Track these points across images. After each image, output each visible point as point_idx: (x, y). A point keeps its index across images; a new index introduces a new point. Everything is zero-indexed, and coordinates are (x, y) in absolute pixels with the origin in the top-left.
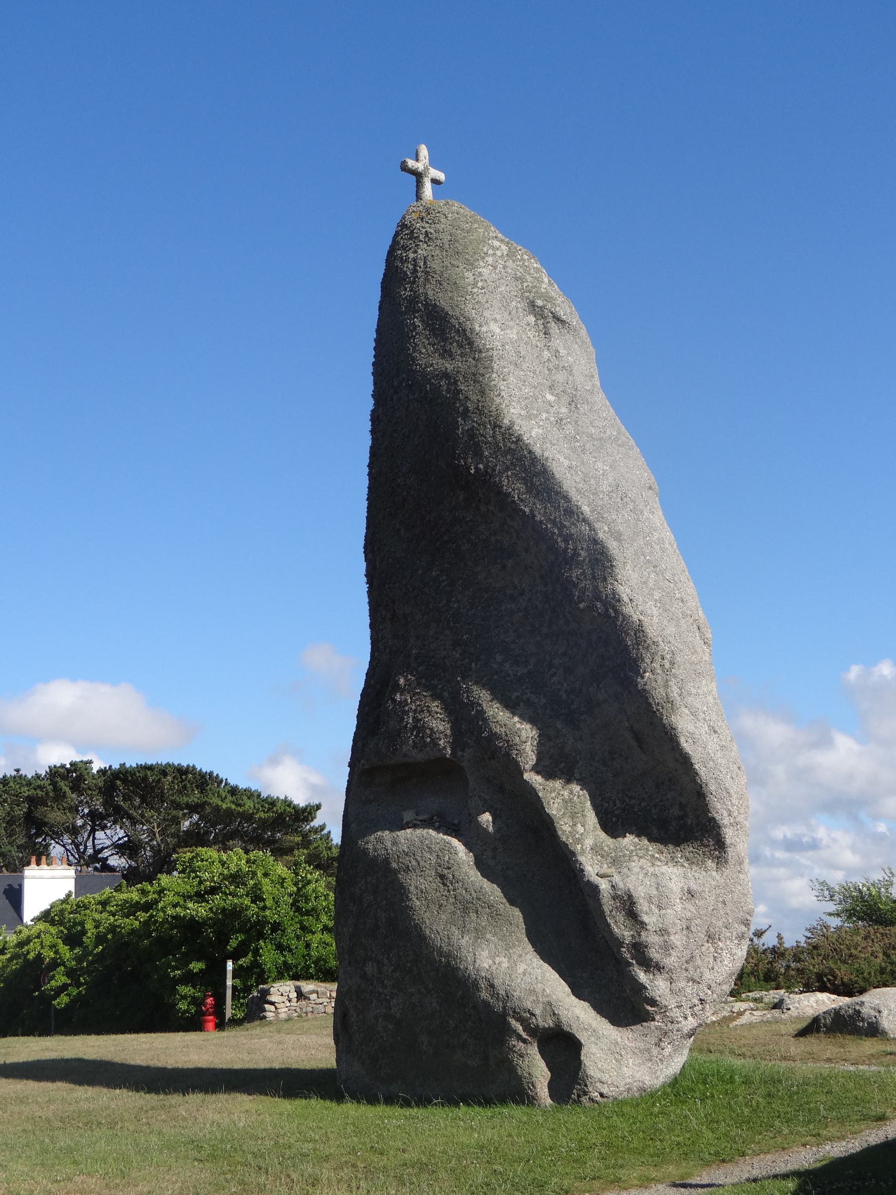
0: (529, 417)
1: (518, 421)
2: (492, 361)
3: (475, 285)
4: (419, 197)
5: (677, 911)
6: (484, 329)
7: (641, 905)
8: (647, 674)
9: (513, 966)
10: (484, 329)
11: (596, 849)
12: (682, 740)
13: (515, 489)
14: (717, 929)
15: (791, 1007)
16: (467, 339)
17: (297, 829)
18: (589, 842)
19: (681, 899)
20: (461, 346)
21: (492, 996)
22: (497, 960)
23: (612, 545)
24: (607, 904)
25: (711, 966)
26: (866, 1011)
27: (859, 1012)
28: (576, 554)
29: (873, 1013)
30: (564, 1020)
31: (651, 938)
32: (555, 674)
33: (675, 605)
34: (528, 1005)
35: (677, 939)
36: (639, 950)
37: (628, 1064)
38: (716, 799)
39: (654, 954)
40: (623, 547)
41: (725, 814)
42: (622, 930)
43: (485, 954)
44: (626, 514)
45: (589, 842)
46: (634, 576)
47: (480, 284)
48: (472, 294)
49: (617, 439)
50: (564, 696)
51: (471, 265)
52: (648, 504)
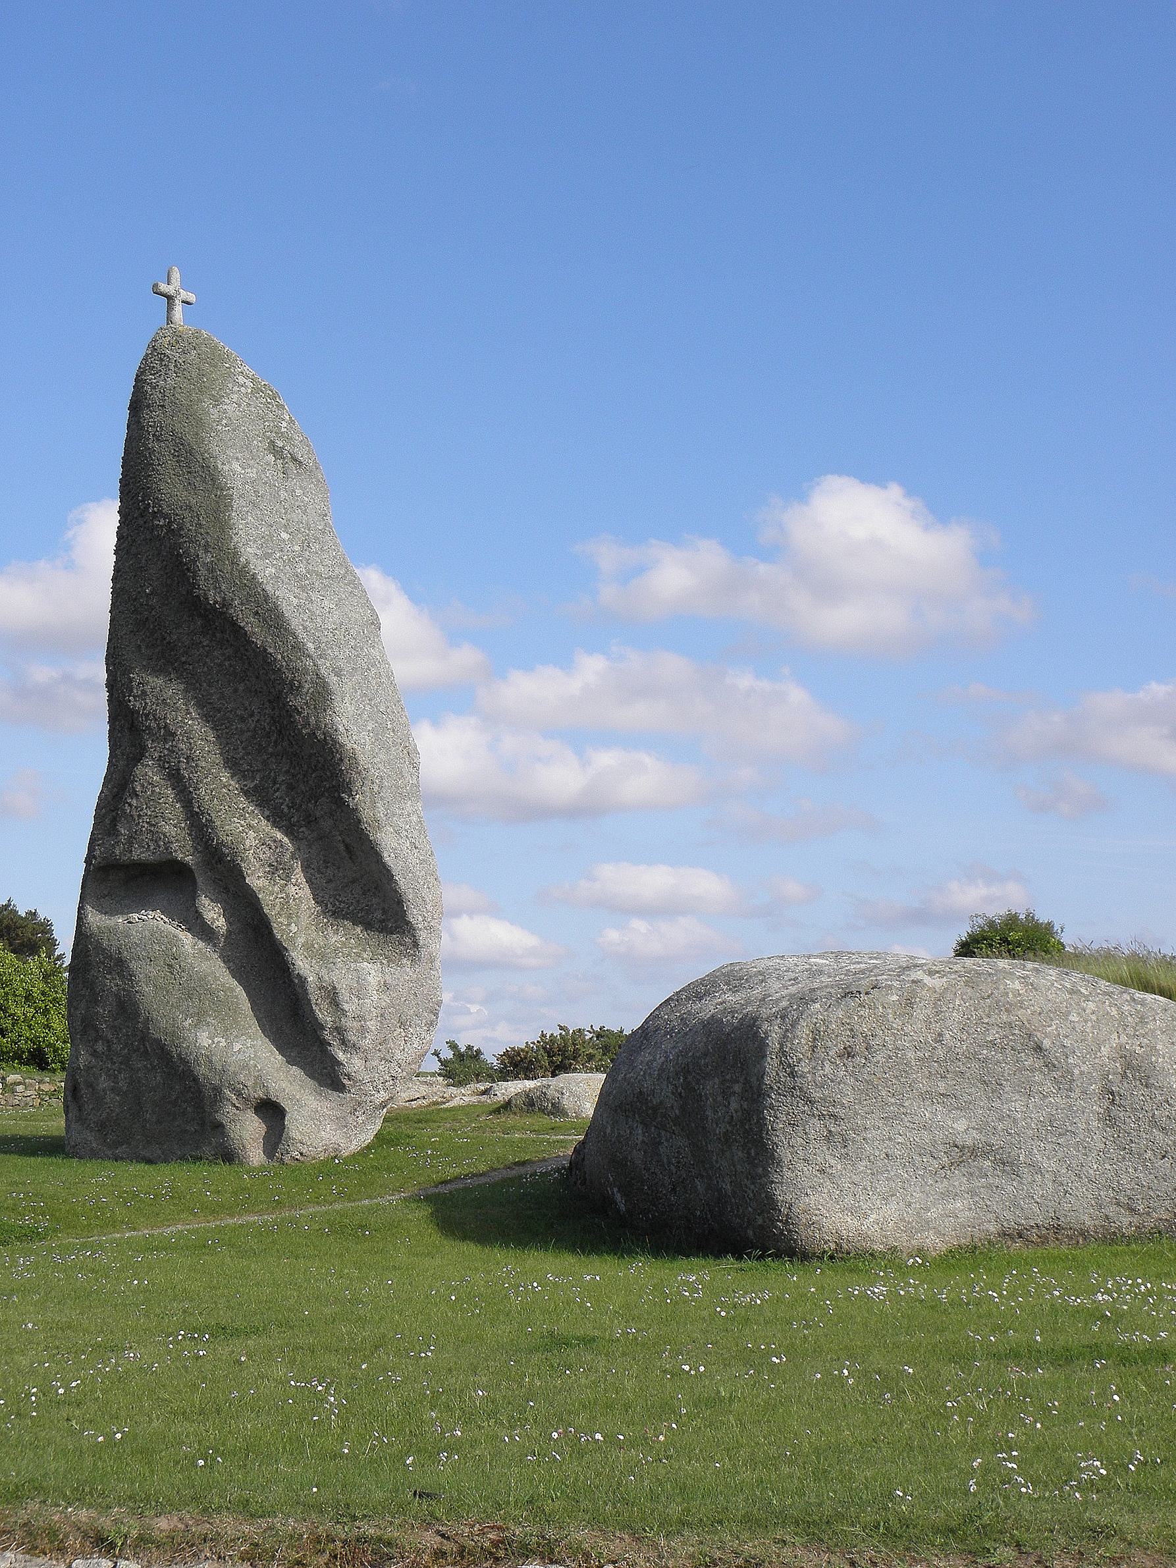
0: (267, 556)
1: (253, 560)
2: (232, 500)
3: (219, 422)
4: (169, 320)
5: (374, 999)
6: (226, 468)
7: (344, 995)
8: (358, 796)
9: (230, 1045)
10: (226, 468)
11: (308, 946)
12: (385, 855)
13: (250, 625)
14: (409, 1017)
15: (497, 1093)
16: (210, 475)
17: (960, 1473)
18: (301, 940)
19: (378, 990)
20: (204, 481)
21: (210, 1070)
22: (216, 1040)
23: (333, 679)
24: (314, 995)
25: (402, 1048)
26: (550, 1093)
27: (545, 1094)
28: (300, 686)
29: (557, 1095)
30: (272, 1091)
31: (348, 1023)
32: (278, 789)
33: (387, 735)
34: (242, 1078)
35: (372, 1025)
36: (339, 1030)
37: (326, 1128)
38: (413, 906)
39: (351, 1037)
40: (342, 681)
41: (420, 919)
42: (323, 1014)
43: (206, 1034)
44: (347, 650)
45: (301, 940)
46: (350, 709)
47: (224, 422)
48: (217, 431)
49: (344, 577)
50: (286, 810)
51: (217, 402)
52: (370, 639)
